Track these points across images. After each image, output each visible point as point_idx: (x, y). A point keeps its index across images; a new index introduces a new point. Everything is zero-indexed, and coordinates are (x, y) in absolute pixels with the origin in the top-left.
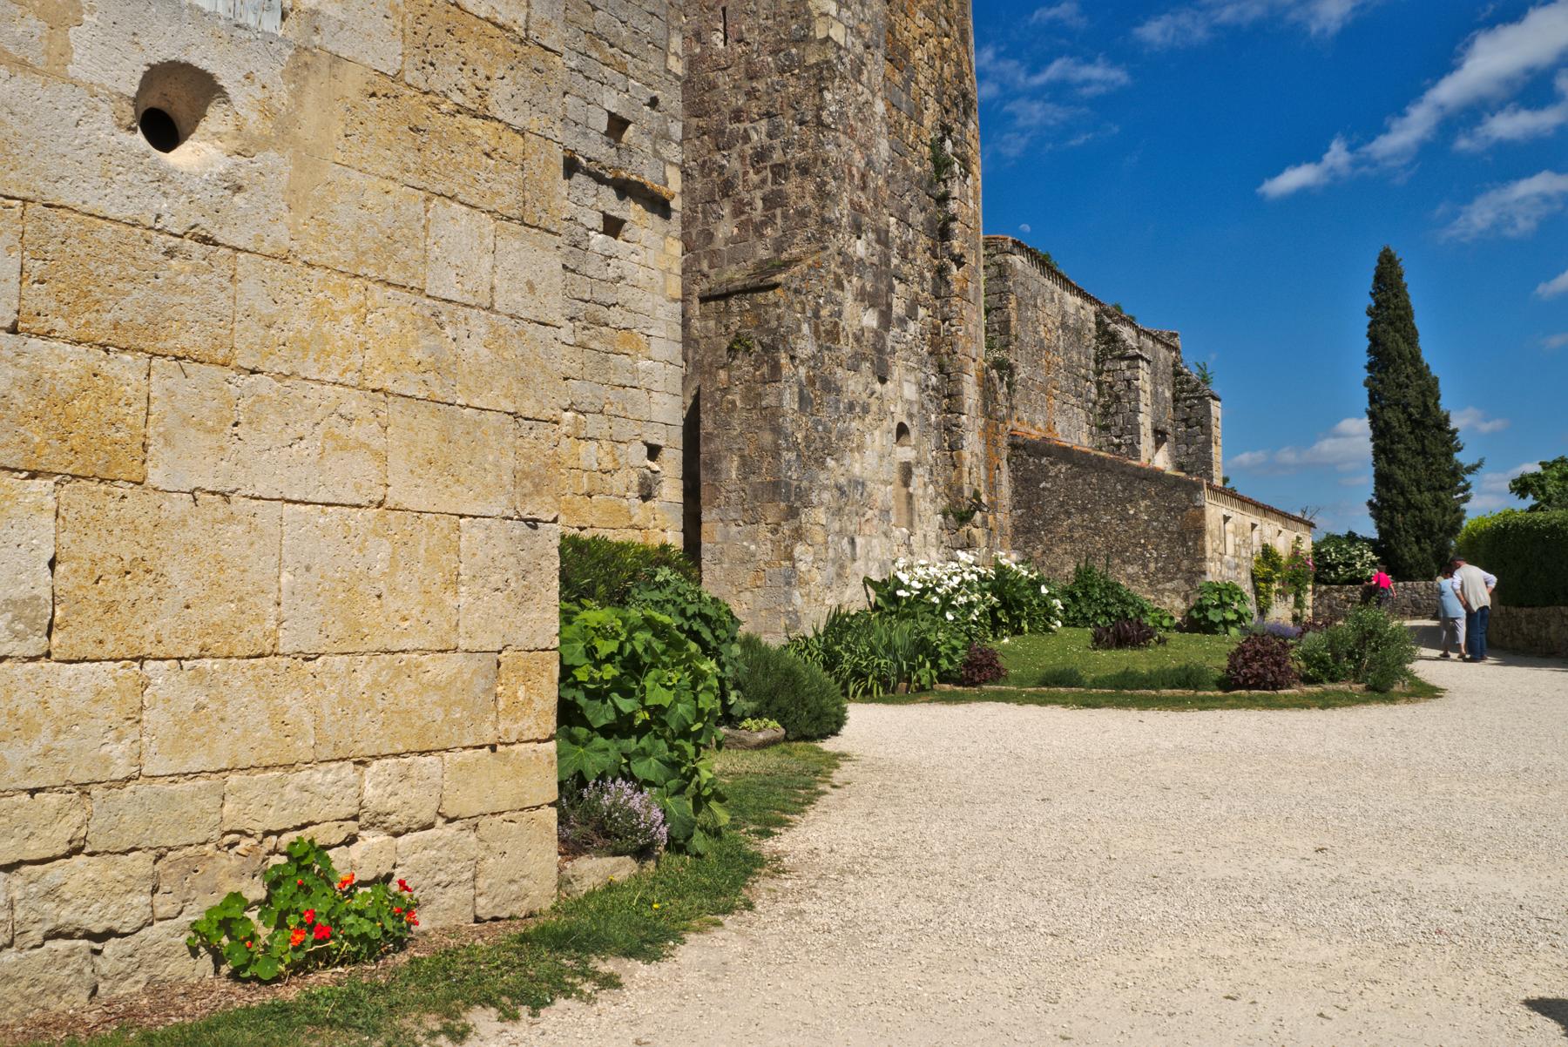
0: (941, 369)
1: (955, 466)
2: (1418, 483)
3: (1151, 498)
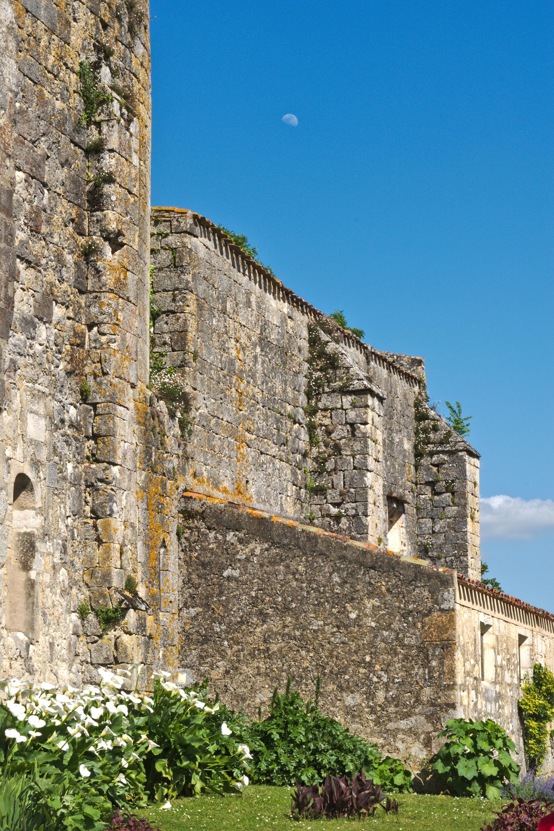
1: (99, 541)
3: (381, 596)
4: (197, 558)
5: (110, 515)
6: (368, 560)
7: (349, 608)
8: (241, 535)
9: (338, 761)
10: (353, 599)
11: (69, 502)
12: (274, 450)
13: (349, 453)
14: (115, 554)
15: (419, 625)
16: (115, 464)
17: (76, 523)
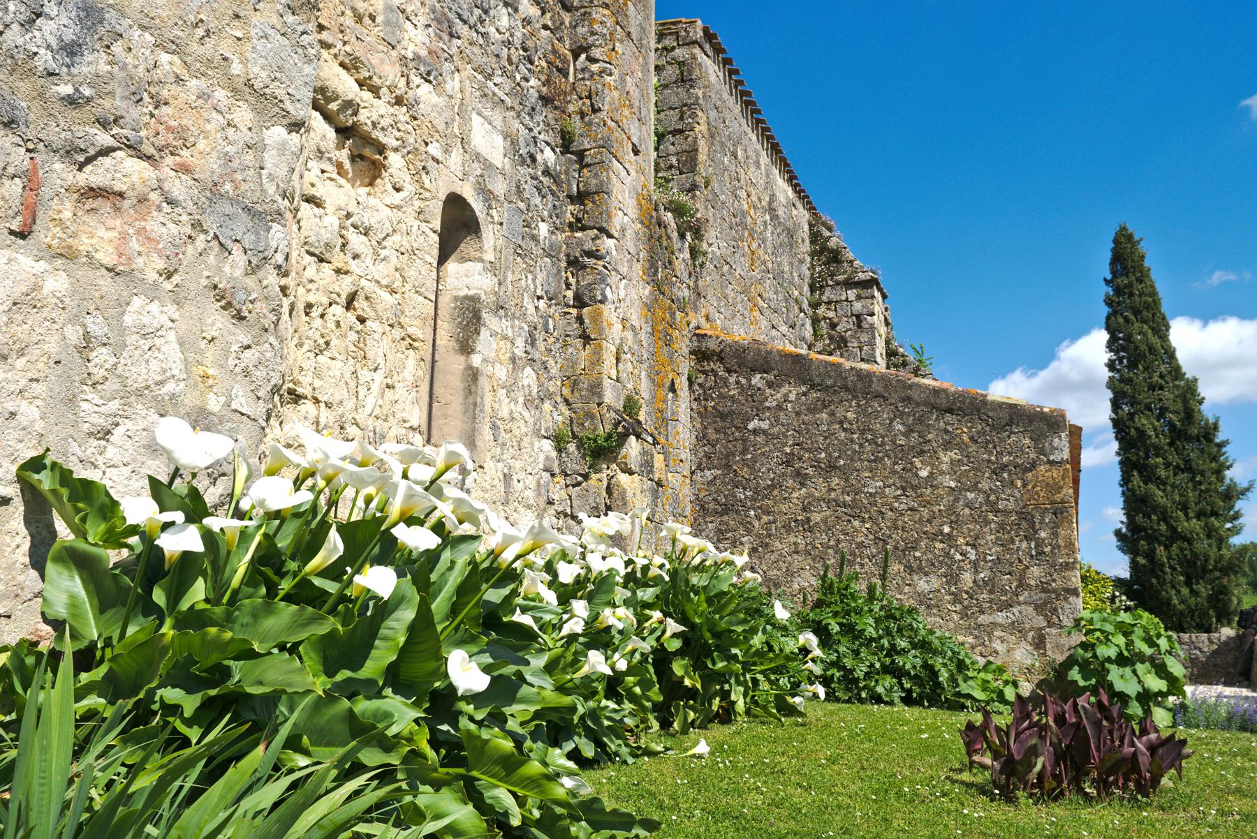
0: (566, 143)
1: (586, 338)
2: (1184, 508)
3: (962, 447)
4: (713, 407)
5: (601, 302)
7: (919, 465)
8: (770, 377)
9: (926, 666)
10: (922, 452)
11: (541, 277)
12: (784, 329)
13: (856, 345)
14: (609, 359)
15: (1019, 483)
16: (610, 236)
17: (552, 310)
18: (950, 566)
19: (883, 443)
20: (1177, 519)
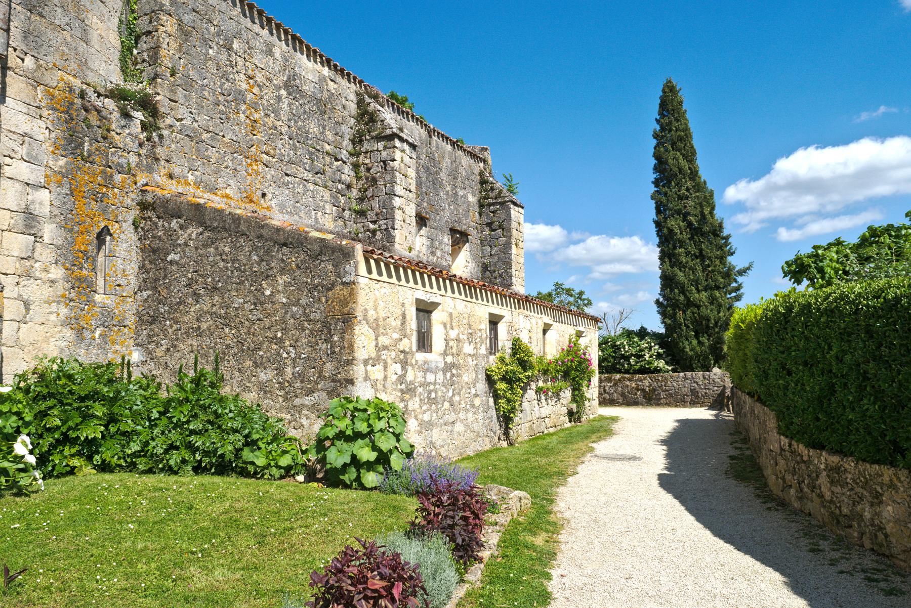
2: (696, 283)
3: (291, 272)
4: (149, 245)
6: (281, 238)
7: (265, 286)
10: (268, 276)
15: (324, 300)
18: (279, 362)
19: (245, 271)
20: (690, 292)
